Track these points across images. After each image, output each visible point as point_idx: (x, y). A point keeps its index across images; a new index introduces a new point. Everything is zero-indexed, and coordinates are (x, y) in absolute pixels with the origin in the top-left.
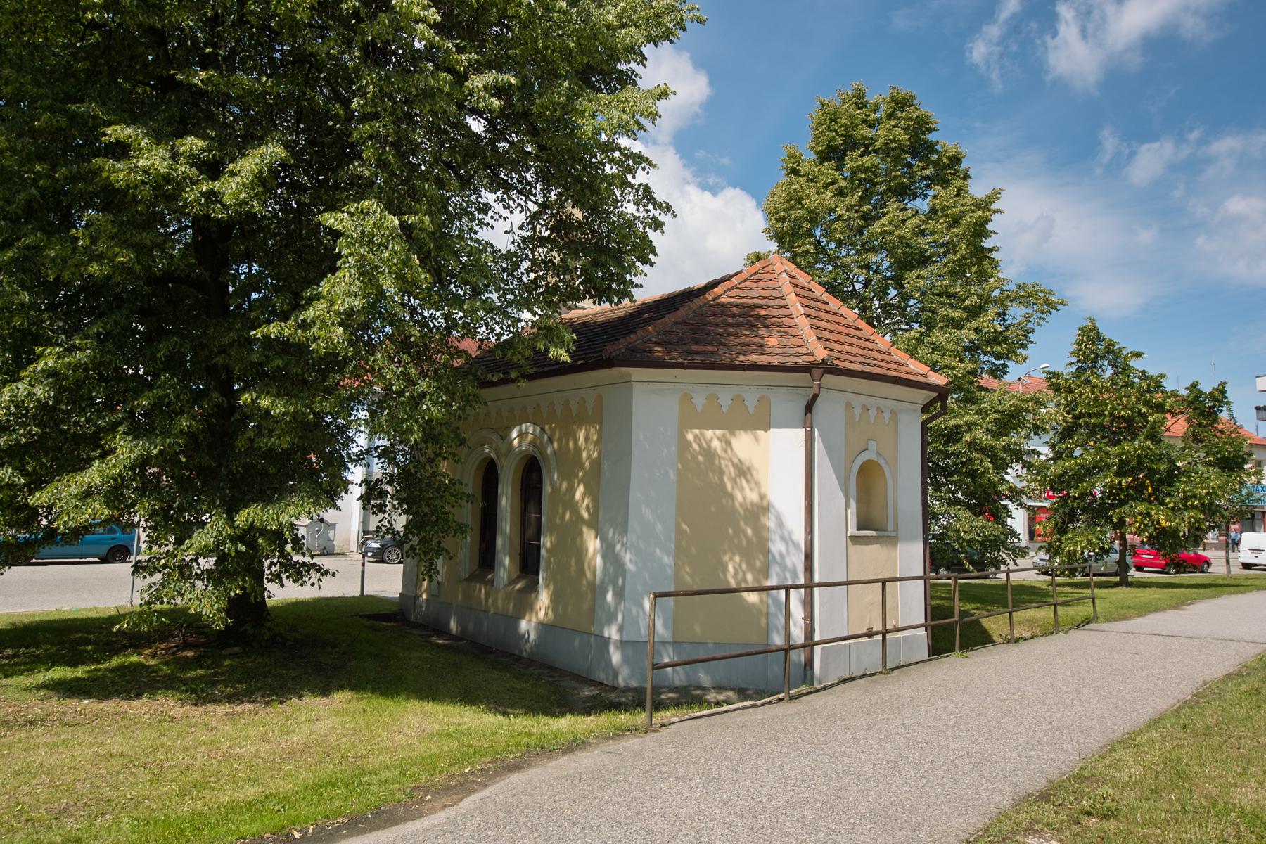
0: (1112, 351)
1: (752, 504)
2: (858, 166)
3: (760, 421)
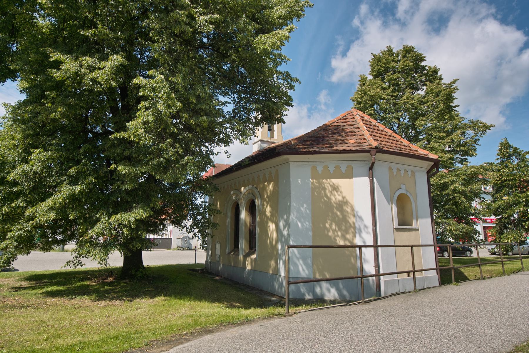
0: (516, 151)
1: (339, 201)
2: (391, 78)
3: (349, 175)
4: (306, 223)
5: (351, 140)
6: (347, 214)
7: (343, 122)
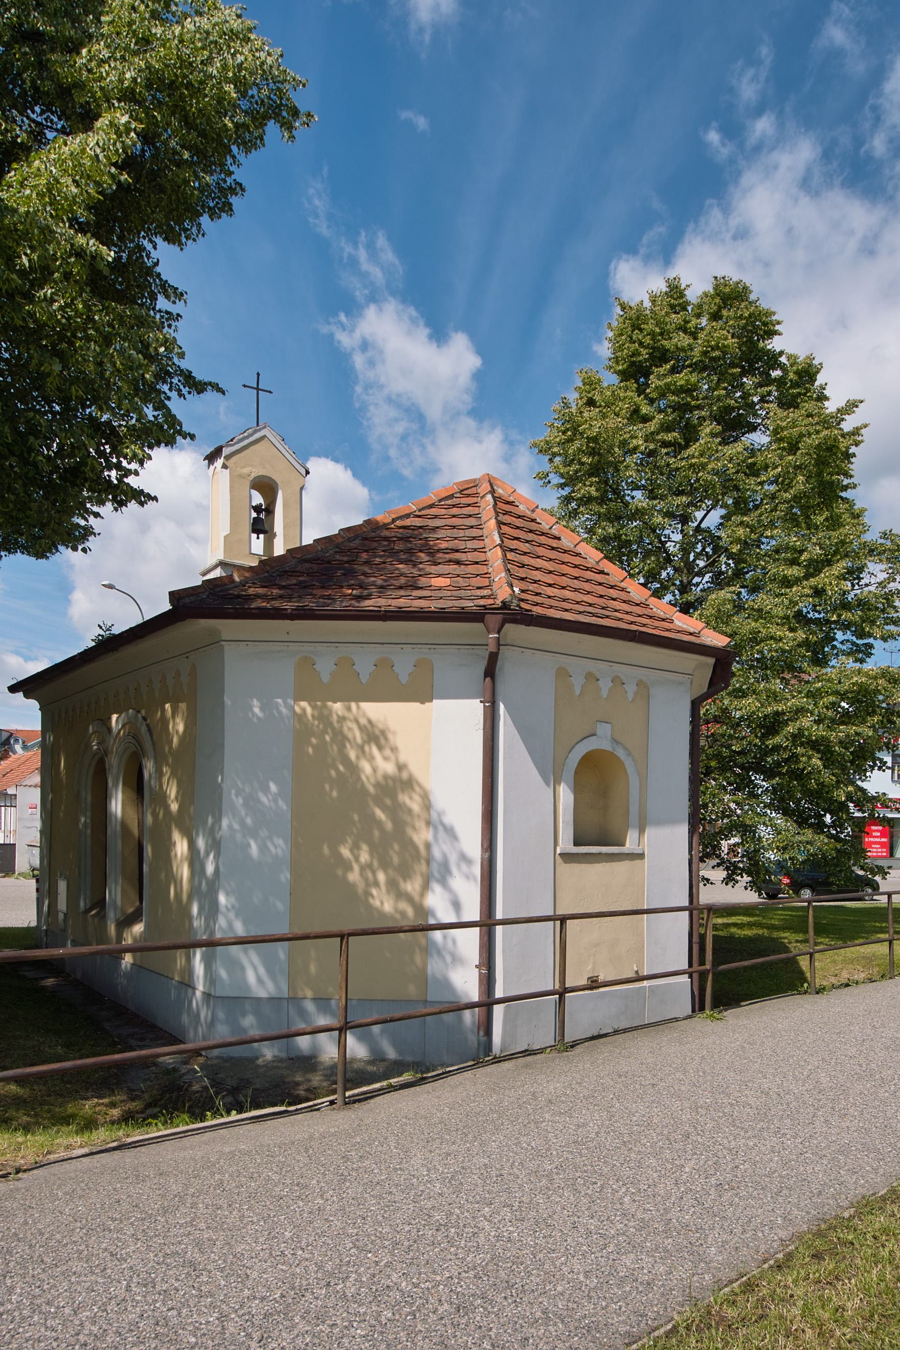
1: (386, 777)
3: (423, 695)
4: (273, 842)
5: (439, 576)
6: (408, 819)
7: (436, 517)
